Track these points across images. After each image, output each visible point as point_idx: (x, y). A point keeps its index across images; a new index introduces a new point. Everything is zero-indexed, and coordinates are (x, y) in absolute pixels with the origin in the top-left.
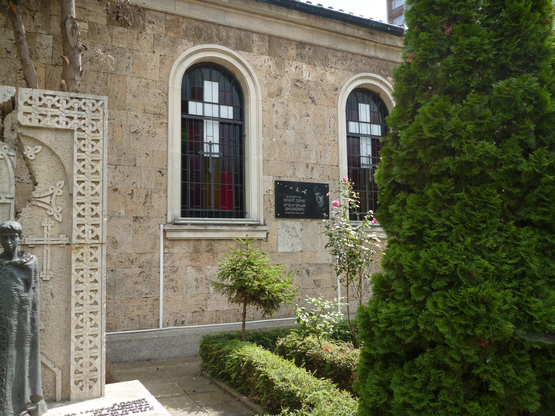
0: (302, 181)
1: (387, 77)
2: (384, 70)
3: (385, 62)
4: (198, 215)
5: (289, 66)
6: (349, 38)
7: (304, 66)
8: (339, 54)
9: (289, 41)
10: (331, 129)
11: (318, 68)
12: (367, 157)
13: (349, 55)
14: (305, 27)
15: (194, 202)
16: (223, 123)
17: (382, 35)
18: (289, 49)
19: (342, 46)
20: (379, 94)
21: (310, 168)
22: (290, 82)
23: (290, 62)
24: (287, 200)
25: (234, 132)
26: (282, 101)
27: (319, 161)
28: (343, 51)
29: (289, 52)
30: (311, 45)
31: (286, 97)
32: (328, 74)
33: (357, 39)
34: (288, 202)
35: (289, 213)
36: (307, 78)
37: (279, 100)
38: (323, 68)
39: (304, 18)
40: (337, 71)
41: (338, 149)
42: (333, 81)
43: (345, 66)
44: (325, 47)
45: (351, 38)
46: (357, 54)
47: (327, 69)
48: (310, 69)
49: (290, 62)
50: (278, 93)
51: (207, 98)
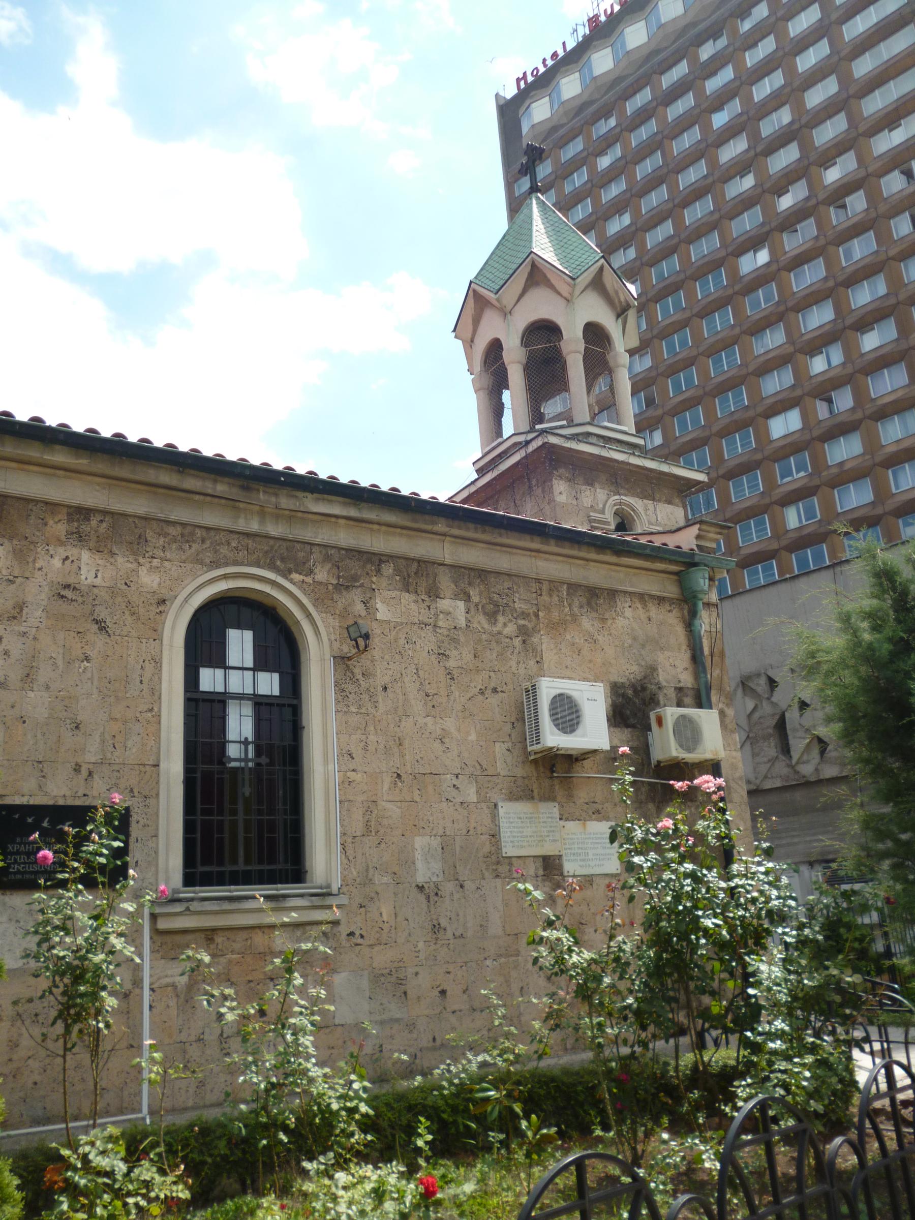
0: (61, 802)
1: (290, 572)
2: (283, 559)
3: (285, 544)
4: (220, 880)
5: (47, 557)
6: (197, 497)
7: (86, 556)
8: (174, 531)
9: (52, 506)
10: (145, 686)
11: (120, 560)
12: (240, 742)
13: (199, 532)
14: (90, 478)
15: (207, 859)
16: (260, 703)
17: (271, 491)
18: (51, 522)
19: (181, 513)
20: (274, 609)
21: (84, 773)
22: (46, 589)
23: (50, 548)
24: (16, 847)
25: (282, 721)
26: (22, 629)
27: (109, 755)
28: (184, 525)
29: (48, 528)
30: (105, 512)
31: (33, 622)
32: (143, 571)
33: (216, 500)
34: (18, 853)
35: (19, 877)
36: (89, 581)
37: (16, 628)
38: (131, 558)
39: (85, 461)
40: (166, 564)
41: (159, 730)
42: (155, 585)
43: (189, 552)
44: (139, 517)
45: (202, 497)
46: (217, 530)
47: (141, 560)
48: (100, 562)
49: (50, 548)
50: (14, 613)
51: (233, 658)
